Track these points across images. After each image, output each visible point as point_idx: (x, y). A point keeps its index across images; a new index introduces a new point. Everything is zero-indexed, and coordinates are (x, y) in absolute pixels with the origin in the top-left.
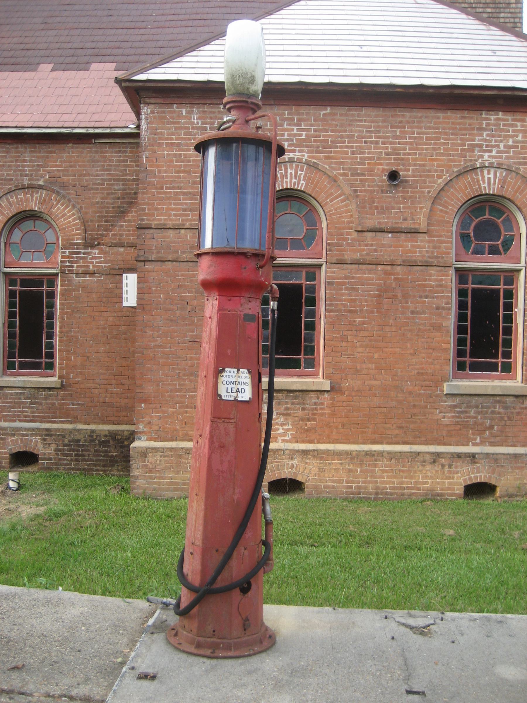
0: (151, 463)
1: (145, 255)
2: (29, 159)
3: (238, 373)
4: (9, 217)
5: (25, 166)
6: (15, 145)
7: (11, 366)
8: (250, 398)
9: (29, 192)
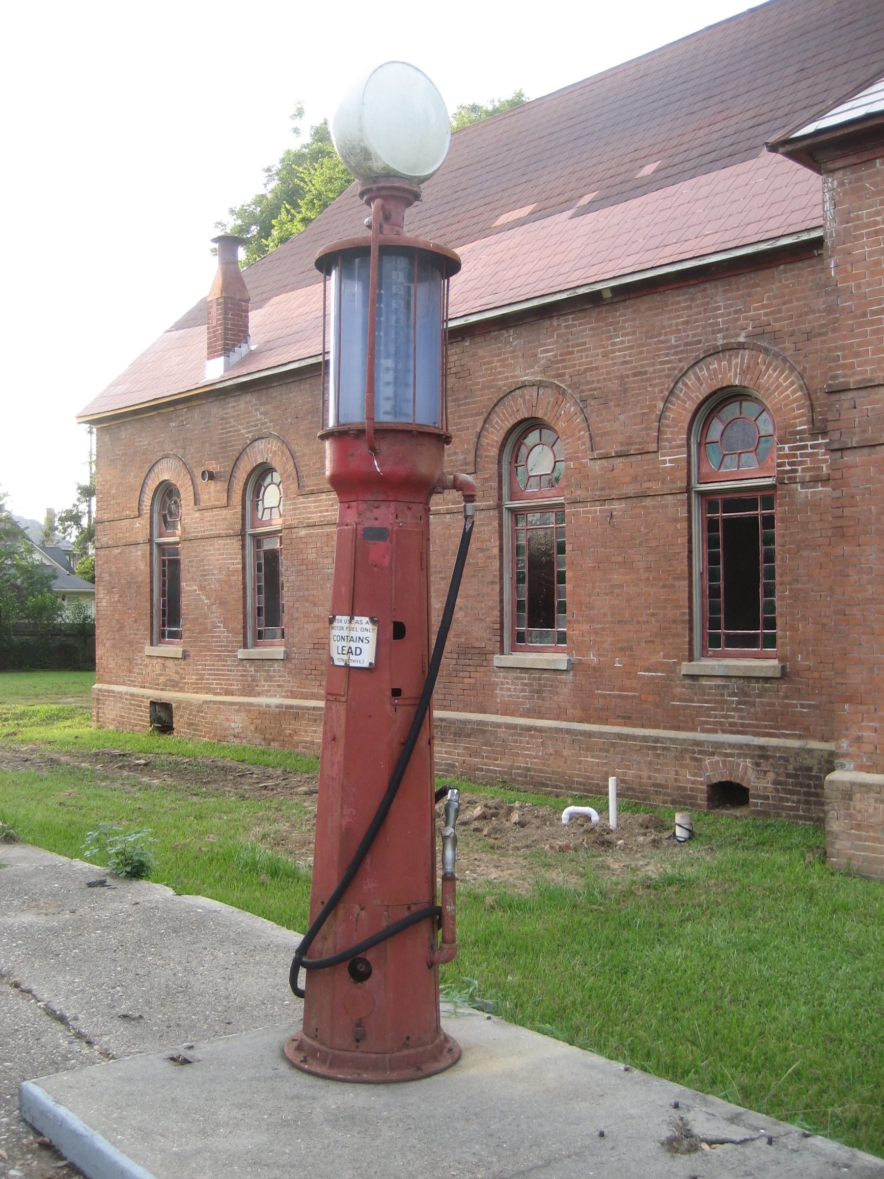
0: (859, 811)
1: (843, 439)
2: (722, 304)
3: (350, 622)
4: (699, 402)
5: (717, 316)
6: (702, 287)
7: (714, 641)
8: (371, 664)
9: (724, 357)
